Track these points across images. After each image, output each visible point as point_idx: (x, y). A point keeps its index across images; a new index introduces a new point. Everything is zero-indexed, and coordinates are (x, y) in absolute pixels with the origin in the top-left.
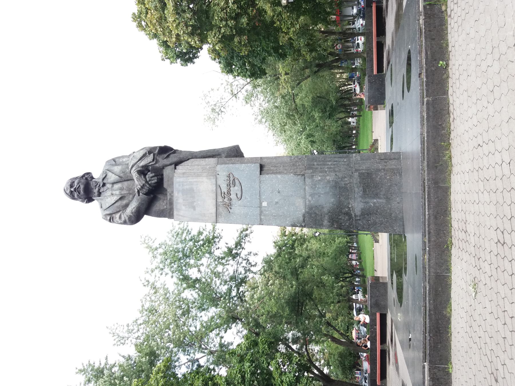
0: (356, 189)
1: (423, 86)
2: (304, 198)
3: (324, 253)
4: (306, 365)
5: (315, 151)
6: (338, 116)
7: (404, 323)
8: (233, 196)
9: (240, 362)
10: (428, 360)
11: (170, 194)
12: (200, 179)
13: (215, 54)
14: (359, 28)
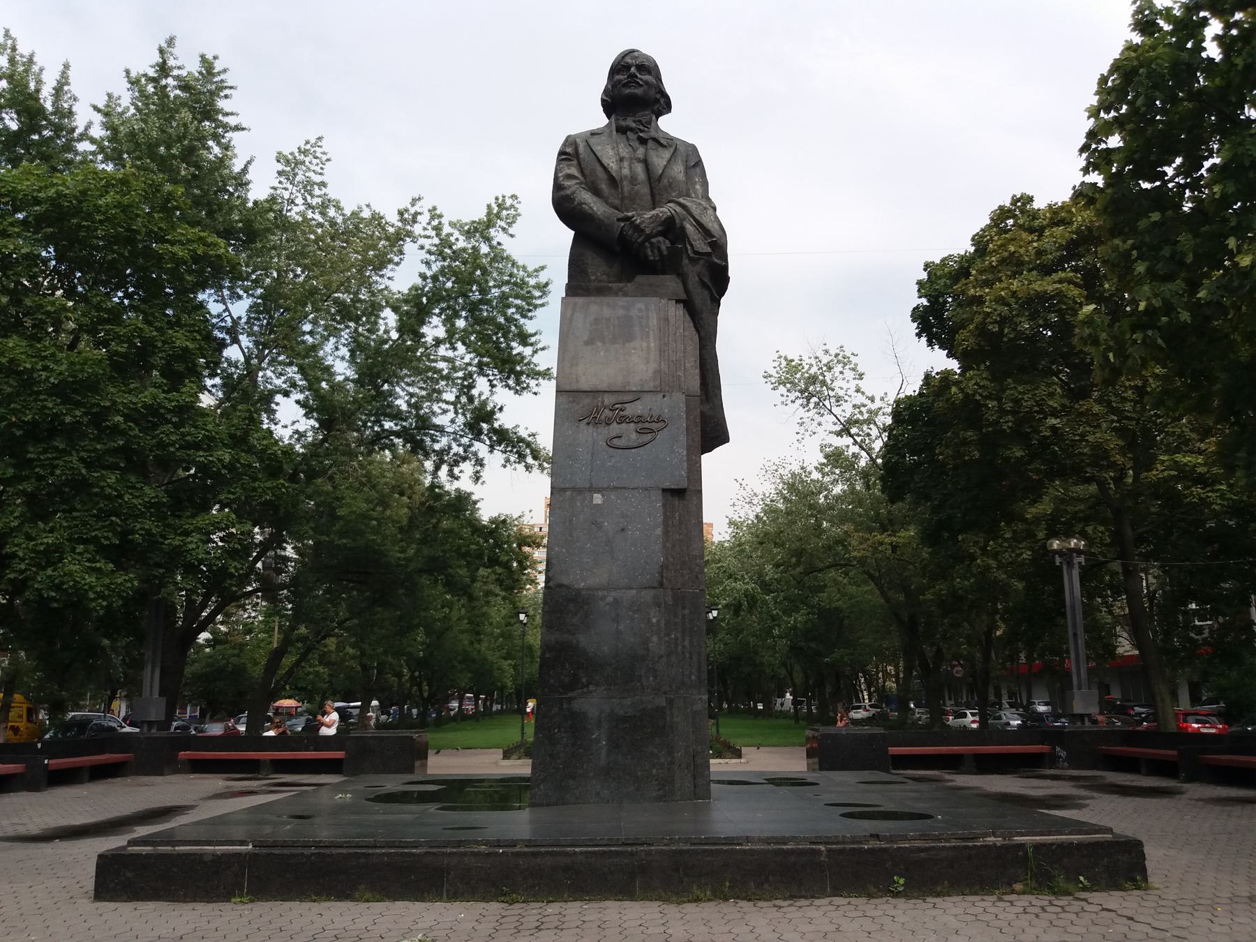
0: (628, 702)
1: (853, 843)
2: (608, 587)
3: (478, 633)
4: (223, 588)
5: (715, 613)
6: (797, 668)
7: (333, 805)
8: (615, 429)
9: (232, 436)
10: (257, 851)
11: (620, 289)
12: (654, 355)
13: (936, 385)
14: (1000, 718)
